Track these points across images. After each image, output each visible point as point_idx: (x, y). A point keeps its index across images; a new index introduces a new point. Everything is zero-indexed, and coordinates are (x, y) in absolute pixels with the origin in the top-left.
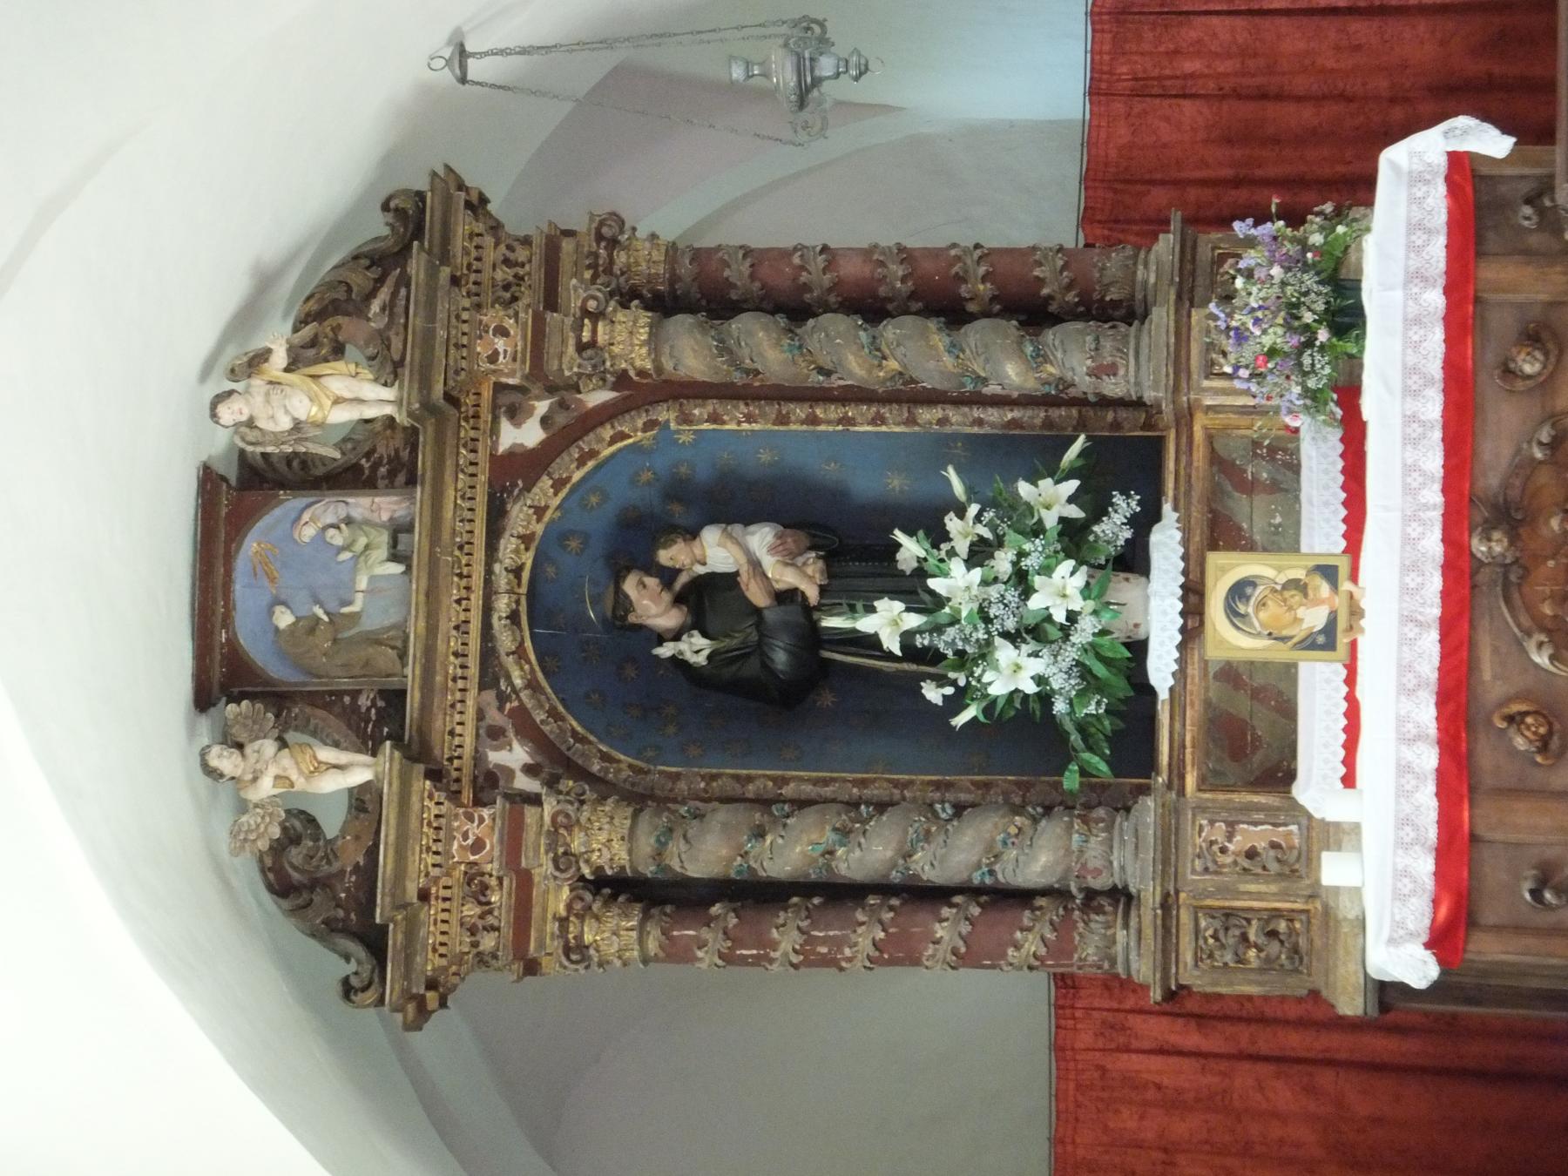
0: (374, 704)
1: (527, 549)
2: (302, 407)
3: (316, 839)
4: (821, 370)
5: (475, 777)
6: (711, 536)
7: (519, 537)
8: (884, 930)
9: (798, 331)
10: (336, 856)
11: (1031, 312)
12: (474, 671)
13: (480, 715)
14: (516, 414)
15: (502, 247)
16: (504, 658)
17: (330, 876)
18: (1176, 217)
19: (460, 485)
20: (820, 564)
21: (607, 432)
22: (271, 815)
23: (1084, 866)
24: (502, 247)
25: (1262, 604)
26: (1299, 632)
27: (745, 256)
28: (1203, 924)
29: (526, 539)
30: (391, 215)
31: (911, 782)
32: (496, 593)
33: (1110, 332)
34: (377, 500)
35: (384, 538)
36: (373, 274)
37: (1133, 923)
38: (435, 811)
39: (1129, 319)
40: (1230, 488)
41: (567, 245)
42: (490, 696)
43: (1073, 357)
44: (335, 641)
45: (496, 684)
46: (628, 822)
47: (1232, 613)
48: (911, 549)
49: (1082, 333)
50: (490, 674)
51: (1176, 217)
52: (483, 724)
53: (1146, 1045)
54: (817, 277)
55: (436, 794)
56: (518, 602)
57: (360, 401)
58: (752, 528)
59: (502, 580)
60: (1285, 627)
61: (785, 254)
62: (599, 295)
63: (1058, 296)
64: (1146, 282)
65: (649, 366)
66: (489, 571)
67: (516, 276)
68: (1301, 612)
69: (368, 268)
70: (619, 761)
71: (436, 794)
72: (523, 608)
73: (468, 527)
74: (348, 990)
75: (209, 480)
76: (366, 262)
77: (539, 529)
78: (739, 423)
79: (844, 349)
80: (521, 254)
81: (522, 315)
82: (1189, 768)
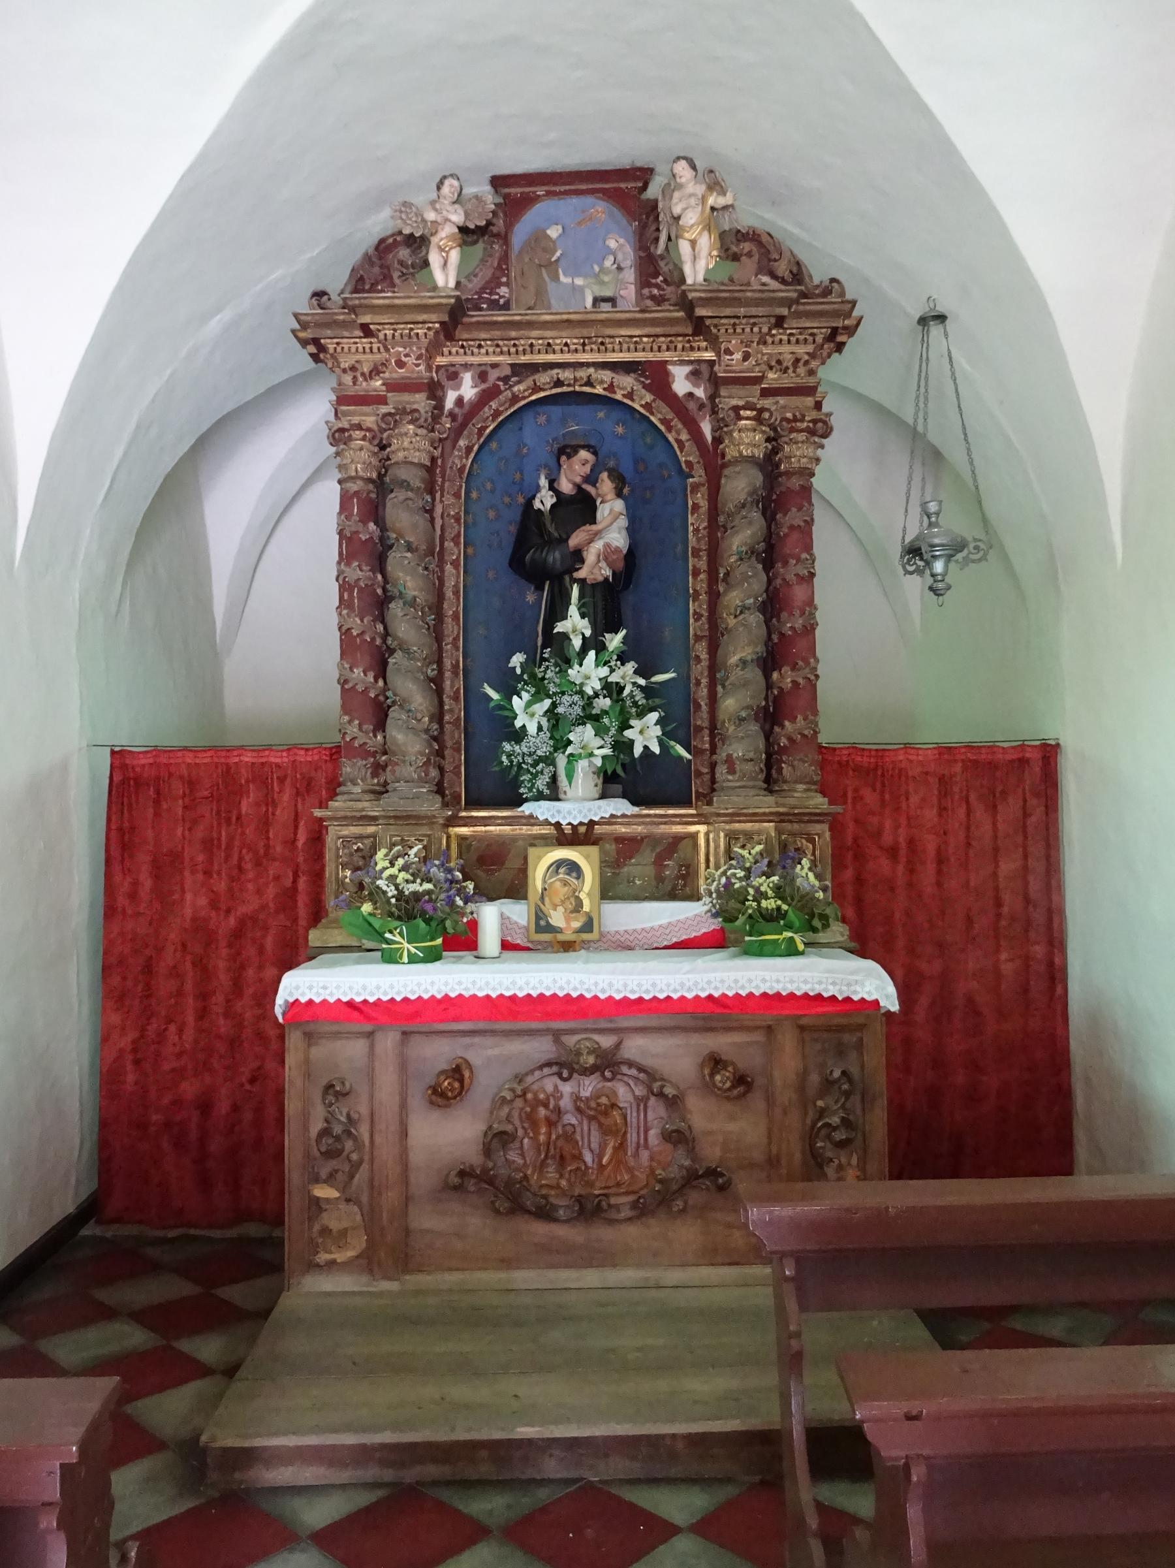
0: (501, 297)
2: (691, 218)
3: (413, 266)
4: (727, 574)
6: (619, 505)
8: (358, 635)
9: (753, 559)
11: (771, 714)
12: (523, 359)
13: (494, 366)
14: (695, 375)
15: (806, 357)
16: (531, 379)
17: (391, 278)
18: (838, 809)
19: (645, 339)
20: (601, 579)
21: (684, 436)
23: (397, 764)
24: (806, 357)
25: (565, 883)
26: (547, 908)
27: (805, 521)
28: (366, 841)
29: (611, 388)
30: (827, 283)
31: (457, 649)
33: (757, 768)
35: (608, 293)
36: (788, 276)
37: (367, 797)
39: (768, 780)
40: (658, 850)
41: (809, 401)
42: (507, 371)
43: (743, 745)
44: (540, 266)
46: (416, 461)
47: (559, 864)
48: (615, 641)
49: (756, 750)
50: (521, 370)
51: (838, 809)
52: (489, 369)
53: (300, 806)
54: (790, 571)
56: (569, 385)
57: (695, 258)
58: (624, 533)
59: (582, 374)
60: (550, 899)
61: (808, 547)
62: (773, 420)
63: (784, 732)
64: (795, 791)
65: (728, 457)
66: (588, 365)
67: (787, 368)
68: (561, 909)
69: (791, 272)
70: (467, 458)
72: (565, 389)
74: (319, 295)
75: (643, 174)
76: (795, 270)
78: (693, 524)
79: (743, 592)
80: (801, 370)
81: (757, 369)
82: (472, 829)
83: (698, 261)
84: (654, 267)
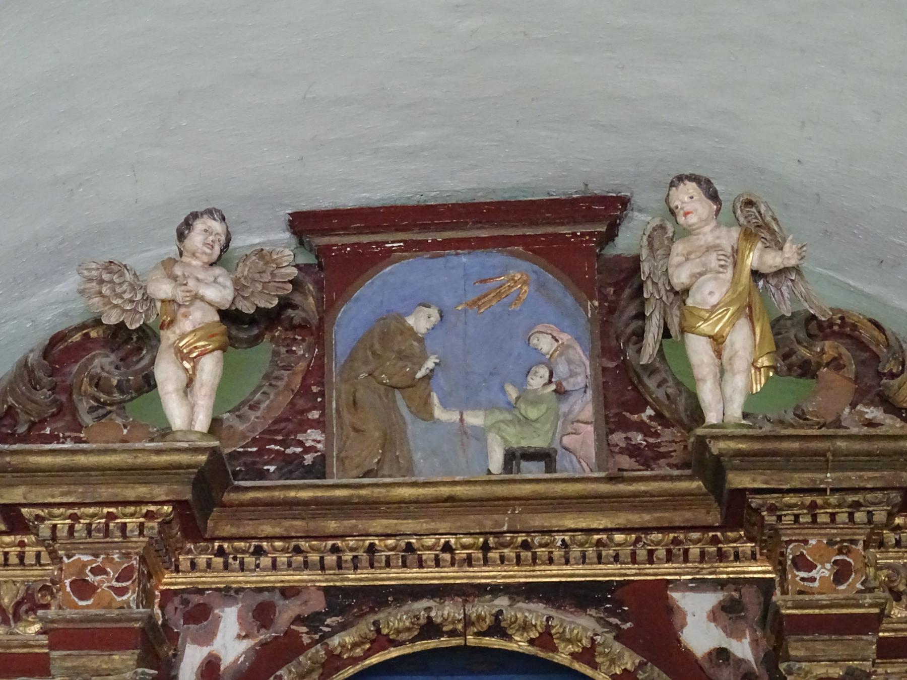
0: (307, 450)
1: (531, 642)
2: (710, 293)
5: (201, 592)
7: (548, 628)
10: (99, 418)
12: (352, 578)
13: (288, 592)
14: (729, 613)
16: (371, 618)
17: (74, 411)
19: (619, 537)
22: (135, 311)
29: (546, 639)
32: (466, 601)
34: (590, 428)
38: (132, 523)
42: (318, 604)
45: (332, 610)
50: (346, 602)
52: (277, 597)
55: (154, 524)
56: (453, 633)
59: (482, 609)
66: (495, 590)
71: (154, 524)
72: (444, 642)
73: (557, 554)
75: (610, 209)
77: (562, 657)
83: (728, 378)
84: (635, 388)
